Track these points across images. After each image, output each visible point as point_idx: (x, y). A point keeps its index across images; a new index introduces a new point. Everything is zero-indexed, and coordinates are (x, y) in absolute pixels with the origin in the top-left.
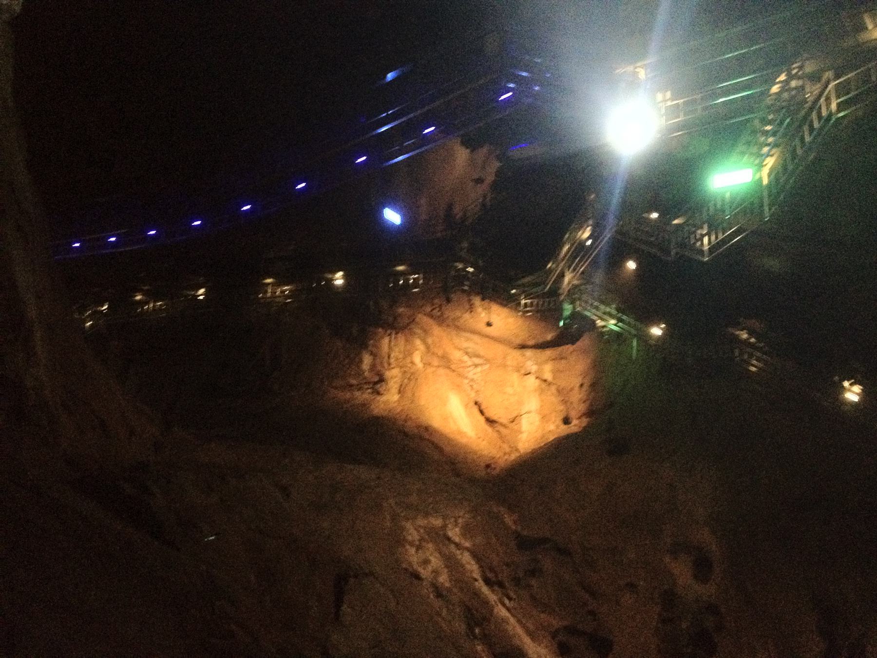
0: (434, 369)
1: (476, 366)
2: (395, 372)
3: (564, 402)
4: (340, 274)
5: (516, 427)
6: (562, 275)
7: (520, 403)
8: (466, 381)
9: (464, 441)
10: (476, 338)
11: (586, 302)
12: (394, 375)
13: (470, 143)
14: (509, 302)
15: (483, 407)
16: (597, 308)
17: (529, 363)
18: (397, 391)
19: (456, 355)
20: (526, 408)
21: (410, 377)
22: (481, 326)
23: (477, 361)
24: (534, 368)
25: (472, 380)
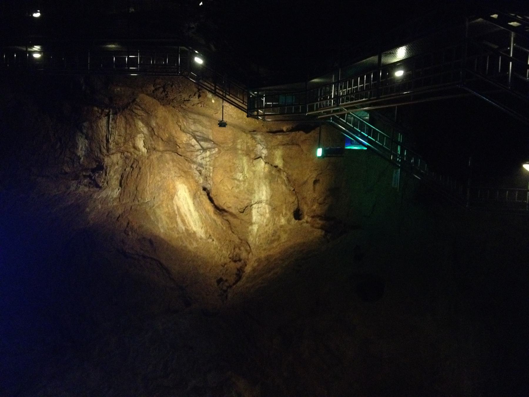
0: (160, 154)
1: (204, 150)
2: (116, 158)
3: (295, 192)
5: (246, 218)
7: (251, 192)
8: (194, 166)
9: (192, 246)
12: (114, 160)
15: (211, 195)
17: (260, 147)
18: (117, 183)
19: (184, 138)
20: (256, 198)
21: (134, 168)
23: (205, 145)
24: (265, 152)
25: (201, 165)
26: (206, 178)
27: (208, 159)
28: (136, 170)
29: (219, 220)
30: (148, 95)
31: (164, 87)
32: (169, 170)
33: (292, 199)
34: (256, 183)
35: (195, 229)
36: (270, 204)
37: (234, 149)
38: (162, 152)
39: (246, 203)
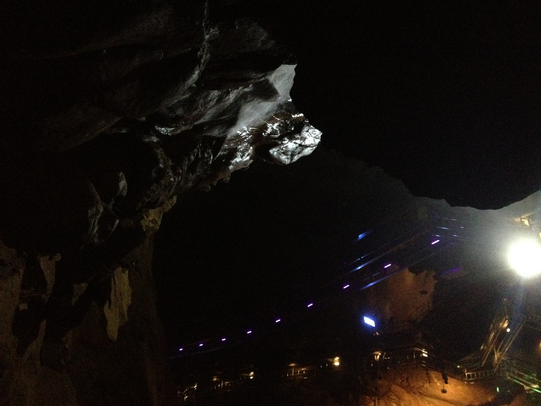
4: (337, 359)
6: (493, 354)
10: (436, 401)
11: (514, 373)
13: (415, 270)
14: (458, 375)
16: (521, 376)
22: (439, 393)
30: (398, 385)
31: (407, 379)
35: (48, 280)
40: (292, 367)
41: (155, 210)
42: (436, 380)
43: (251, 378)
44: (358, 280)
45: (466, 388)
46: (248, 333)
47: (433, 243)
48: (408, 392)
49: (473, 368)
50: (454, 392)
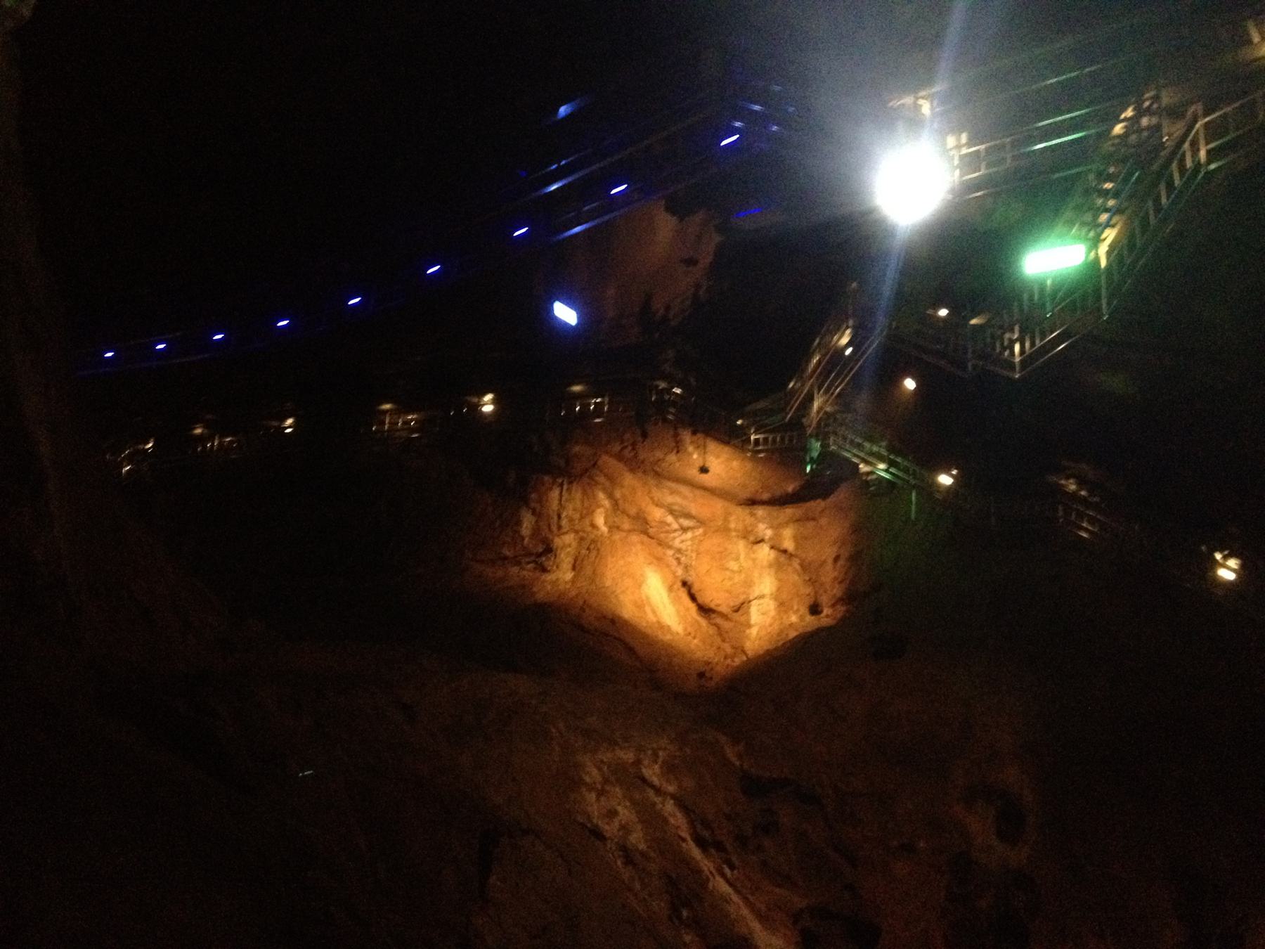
1: (684, 530)
2: (569, 538)
4: (488, 397)
5: (743, 619)
6: (810, 399)
7: (749, 584)
8: (670, 552)
12: (566, 543)
13: (677, 207)
14: (732, 437)
15: (693, 591)
16: (859, 446)
17: (761, 526)
19: (657, 514)
21: (591, 548)
22: (693, 473)
23: (686, 523)
24: (769, 533)
25: (679, 551)
26: (686, 568)
27: (689, 543)
28: (594, 553)
29: (703, 622)
30: (611, 456)
32: (636, 554)
33: (808, 590)
34: (756, 574)
36: (776, 599)
37: (725, 530)
38: (630, 531)
39: (742, 598)
40: (386, 412)
41: (832, 499)
42: (691, 449)
43: (289, 430)
44: (548, 216)
45: (749, 465)
46: (285, 322)
47: (724, 143)
48: (632, 470)
49: (767, 425)
50: (724, 475)
